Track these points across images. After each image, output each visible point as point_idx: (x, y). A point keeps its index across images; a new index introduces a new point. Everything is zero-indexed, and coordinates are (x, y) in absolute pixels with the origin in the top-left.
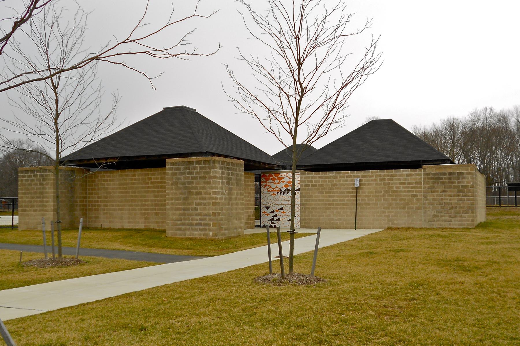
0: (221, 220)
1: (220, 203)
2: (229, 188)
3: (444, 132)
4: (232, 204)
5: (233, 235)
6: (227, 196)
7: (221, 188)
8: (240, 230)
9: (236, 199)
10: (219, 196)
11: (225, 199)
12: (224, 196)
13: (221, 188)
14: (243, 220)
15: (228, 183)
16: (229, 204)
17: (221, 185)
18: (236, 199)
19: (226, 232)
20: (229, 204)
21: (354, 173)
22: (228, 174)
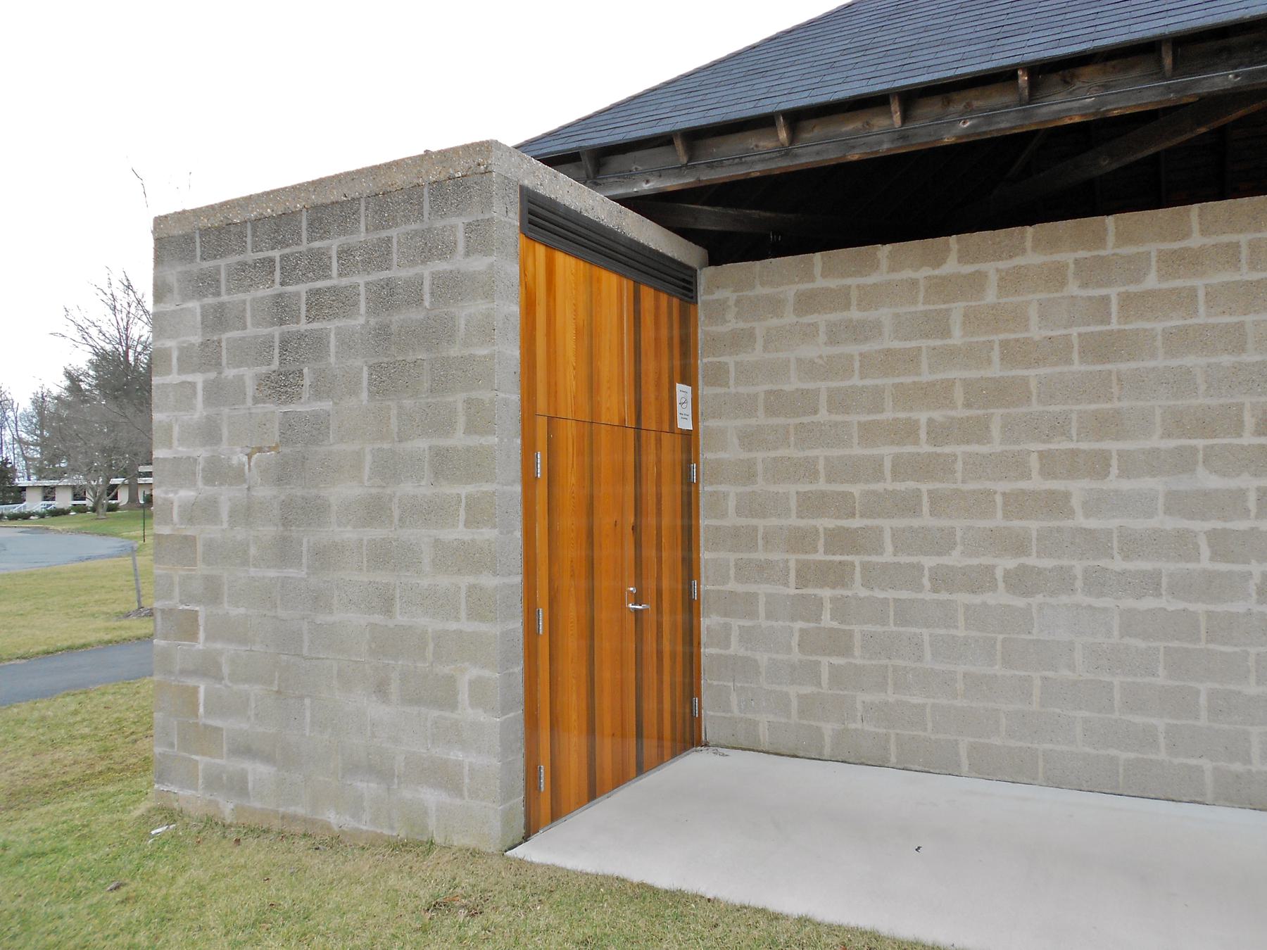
0: (208, 668)
1: (189, 541)
2: (289, 426)
3: (141, 331)
4: (324, 557)
5: (333, 818)
6: (264, 492)
7: (209, 433)
8: (431, 797)
9: (374, 511)
10: (408, 488)
11: (245, 513)
12: (227, 495)
13: (209, 433)
14: (468, 713)
15: (280, 386)
16: (284, 552)
17: (199, 411)
18: (374, 511)
19: (257, 771)
20: (284, 552)
21: (1101, 240)
22: (281, 310)
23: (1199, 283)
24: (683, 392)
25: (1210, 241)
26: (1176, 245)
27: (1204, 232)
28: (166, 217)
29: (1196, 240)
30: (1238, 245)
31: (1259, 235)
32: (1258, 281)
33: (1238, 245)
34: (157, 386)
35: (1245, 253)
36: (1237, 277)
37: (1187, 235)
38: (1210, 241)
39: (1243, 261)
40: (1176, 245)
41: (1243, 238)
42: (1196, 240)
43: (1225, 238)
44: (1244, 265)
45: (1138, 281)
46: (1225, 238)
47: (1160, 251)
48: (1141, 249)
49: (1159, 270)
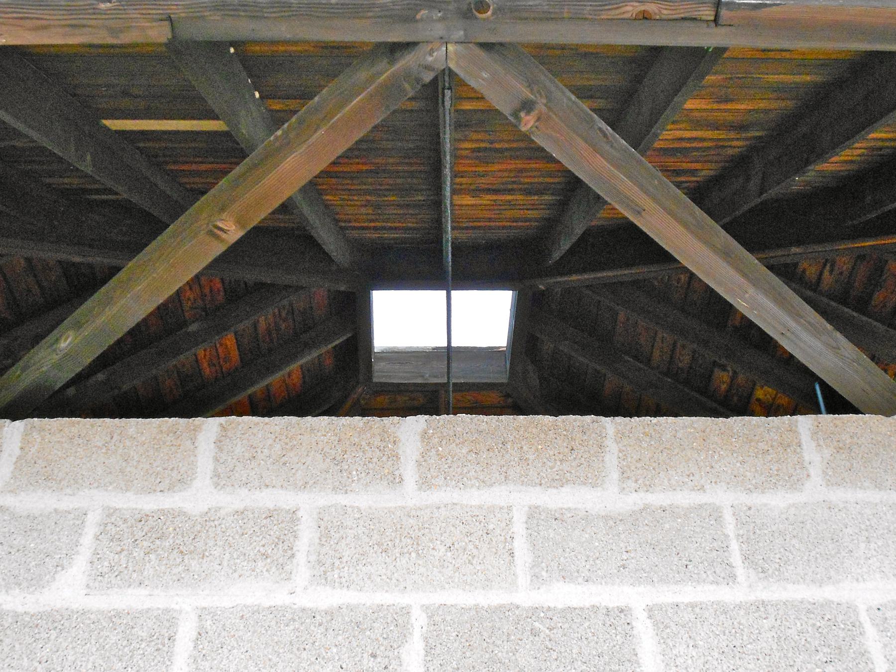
23: (186, 603)
24: (484, 318)
25: (231, 501)
26: (149, 503)
27: (220, 480)
28: (882, 117)
29: (199, 497)
30: (293, 515)
31: (342, 499)
32: (330, 613)
33: (293, 515)
34: (243, 226)
35: (306, 536)
36: (280, 598)
37: (182, 482)
38: (231, 501)
39: (301, 558)
40: (149, 503)
41: (307, 503)
42: (199, 497)
43: (267, 499)
44: (302, 572)
45: (36, 582)
46: (267, 499)
47: (110, 512)
48: (66, 503)
49: (97, 557)
